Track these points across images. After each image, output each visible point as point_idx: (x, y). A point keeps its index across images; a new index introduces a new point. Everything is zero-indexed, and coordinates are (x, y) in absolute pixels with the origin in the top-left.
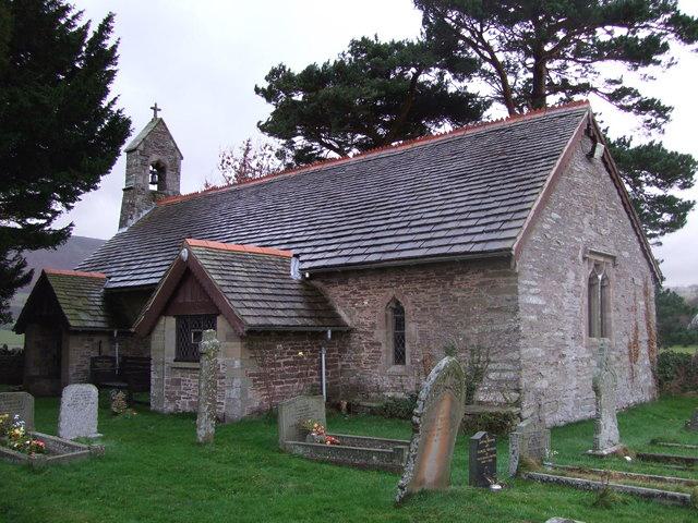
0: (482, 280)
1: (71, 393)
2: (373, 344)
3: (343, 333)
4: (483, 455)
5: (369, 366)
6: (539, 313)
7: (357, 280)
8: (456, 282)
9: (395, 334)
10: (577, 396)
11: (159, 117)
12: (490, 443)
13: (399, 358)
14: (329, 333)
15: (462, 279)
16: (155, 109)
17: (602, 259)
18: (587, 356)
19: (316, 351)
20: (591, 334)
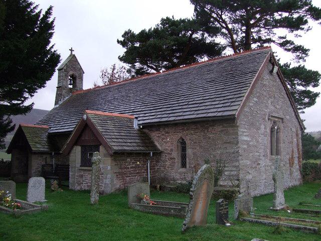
1: (33, 181)
2: (171, 159)
3: (158, 154)
4: (222, 210)
7: (164, 129)
10: (265, 182)
13: (184, 165)
14: (151, 153)
15: (212, 129)
16: (71, 50)
18: (270, 164)
20: (272, 154)
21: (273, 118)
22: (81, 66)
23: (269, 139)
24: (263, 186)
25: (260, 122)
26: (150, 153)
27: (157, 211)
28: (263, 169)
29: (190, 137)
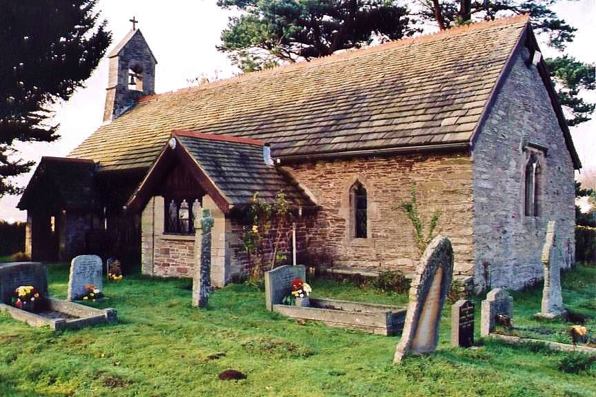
0: (439, 167)
2: (337, 220)
3: (312, 211)
5: (333, 239)
6: (488, 196)
7: (324, 165)
8: (414, 169)
9: (577, 231)
10: (515, 265)
11: (137, 28)
12: (469, 310)
13: (361, 232)
15: (421, 166)
16: (134, 21)
17: (536, 151)
18: (524, 232)
19: (288, 226)
20: (527, 214)
21: (529, 149)
22: (150, 51)
23: (524, 186)
24: (511, 273)
25: (508, 155)
26: (298, 210)
27: (465, 358)
28: (512, 241)
29: (376, 180)
